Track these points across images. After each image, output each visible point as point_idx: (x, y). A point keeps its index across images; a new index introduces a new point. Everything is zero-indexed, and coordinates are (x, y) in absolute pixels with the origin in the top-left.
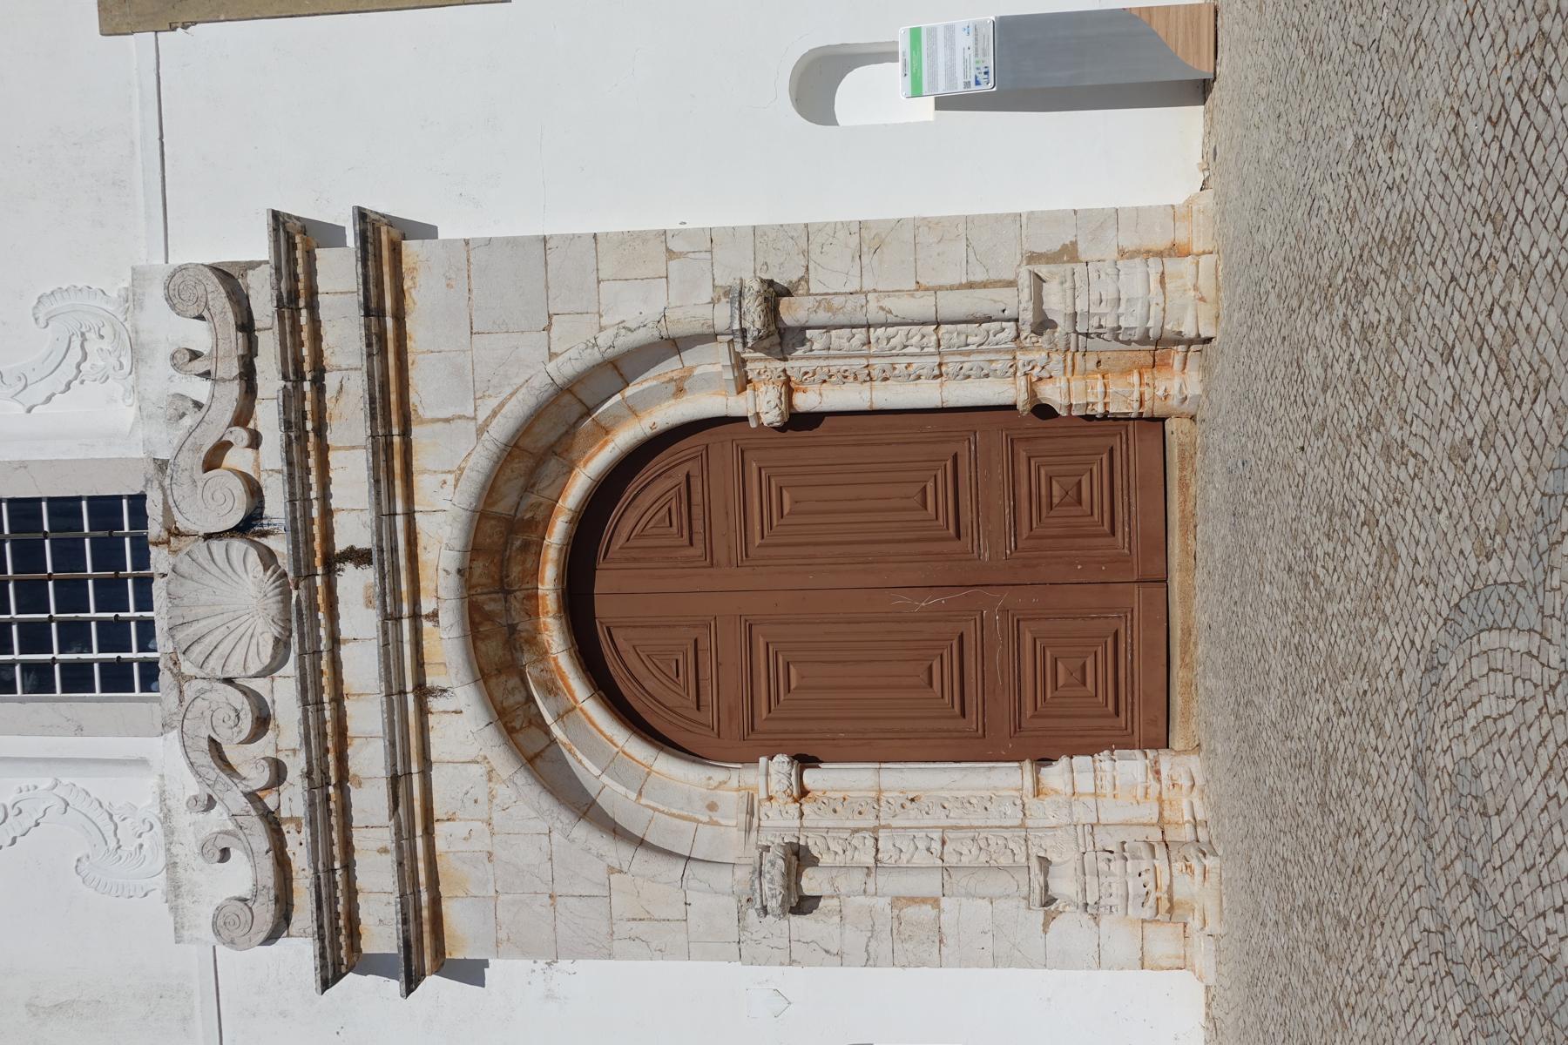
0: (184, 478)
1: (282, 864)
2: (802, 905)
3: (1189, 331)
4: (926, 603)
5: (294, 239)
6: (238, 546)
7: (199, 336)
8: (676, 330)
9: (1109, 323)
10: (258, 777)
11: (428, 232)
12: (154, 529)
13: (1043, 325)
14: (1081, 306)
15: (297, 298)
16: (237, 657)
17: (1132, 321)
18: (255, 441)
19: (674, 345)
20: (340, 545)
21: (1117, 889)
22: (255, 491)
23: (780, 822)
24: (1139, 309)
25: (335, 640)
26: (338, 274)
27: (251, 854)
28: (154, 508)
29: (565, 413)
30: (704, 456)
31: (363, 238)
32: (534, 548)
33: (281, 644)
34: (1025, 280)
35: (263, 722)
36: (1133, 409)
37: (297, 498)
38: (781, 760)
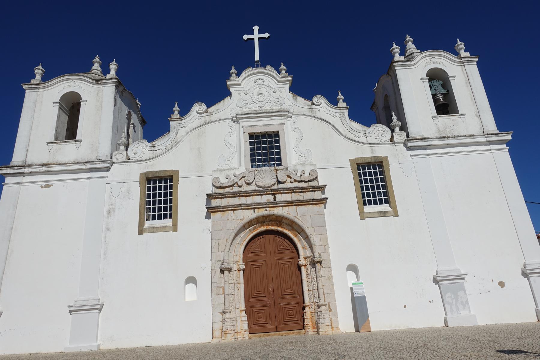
0: (285, 172)
1: (226, 187)
2: (222, 271)
3: (320, 330)
4: (271, 291)
5: (322, 188)
6: (276, 180)
7: (307, 174)
8: (313, 247)
9: (320, 317)
10: (240, 184)
11: (325, 208)
12: (277, 167)
13: (319, 306)
14: (323, 312)
17: (321, 321)
18: (292, 182)
19: (311, 247)
21: (228, 324)
22: (284, 183)
23: (235, 267)
24: (323, 322)
25: (261, 195)
26: (317, 195)
27: (228, 182)
28: (280, 167)
29: (293, 225)
31: (324, 199)
32: (277, 225)
33: (260, 187)
34: (326, 303)
36: (305, 323)
37: (284, 189)
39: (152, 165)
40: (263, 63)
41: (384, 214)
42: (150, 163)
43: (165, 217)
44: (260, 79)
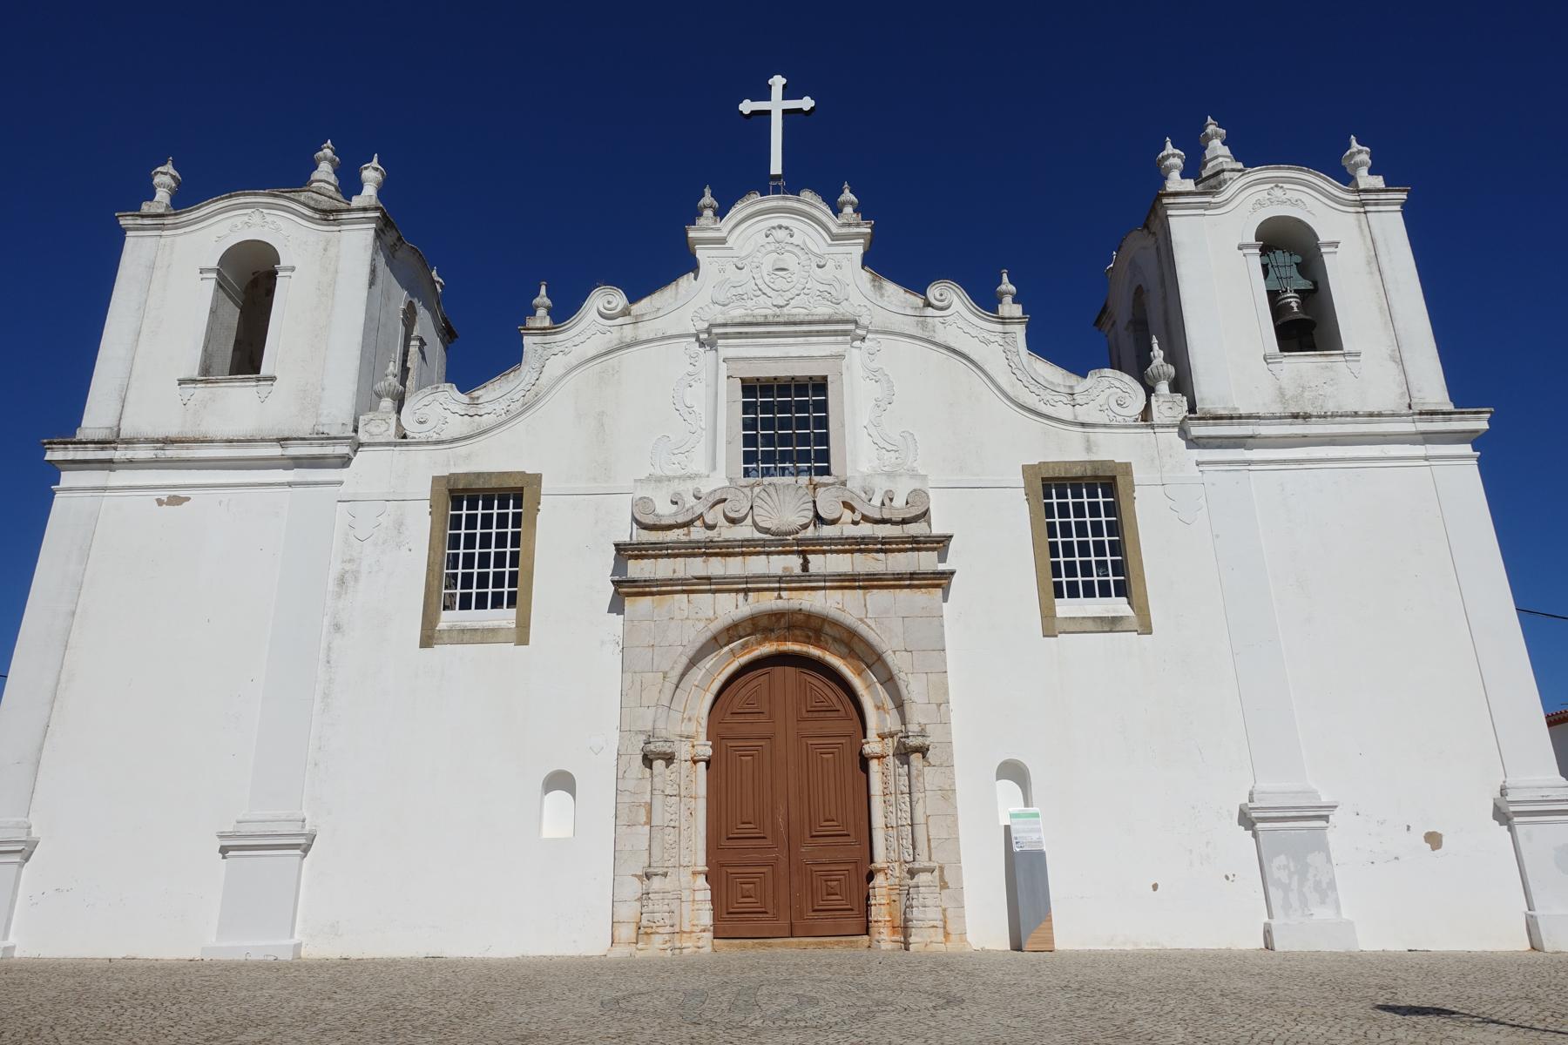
1: (669, 527)
2: (648, 761)
3: (912, 940)
5: (940, 544)
6: (811, 514)
7: (899, 502)
8: (907, 707)
9: (915, 903)
10: (709, 519)
11: (945, 599)
12: (817, 479)
13: (912, 873)
15: (917, 544)
16: (762, 512)
17: (916, 913)
18: (855, 523)
19: (900, 706)
20: (810, 557)
22: (834, 522)
23: (683, 751)
24: (921, 916)
25: (768, 554)
26: (926, 561)
27: (675, 514)
28: (825, 479)
30: (848, 718)
33: (767, 531)
34: (932, 864)
35: (733, 521)
36: (873, 918)
37: (831, 541)
38: (709, 752)
39: (468, 456)
41: (1111, 624)
42: (462, 449)
43: (497, 602)
44: (780, 227)
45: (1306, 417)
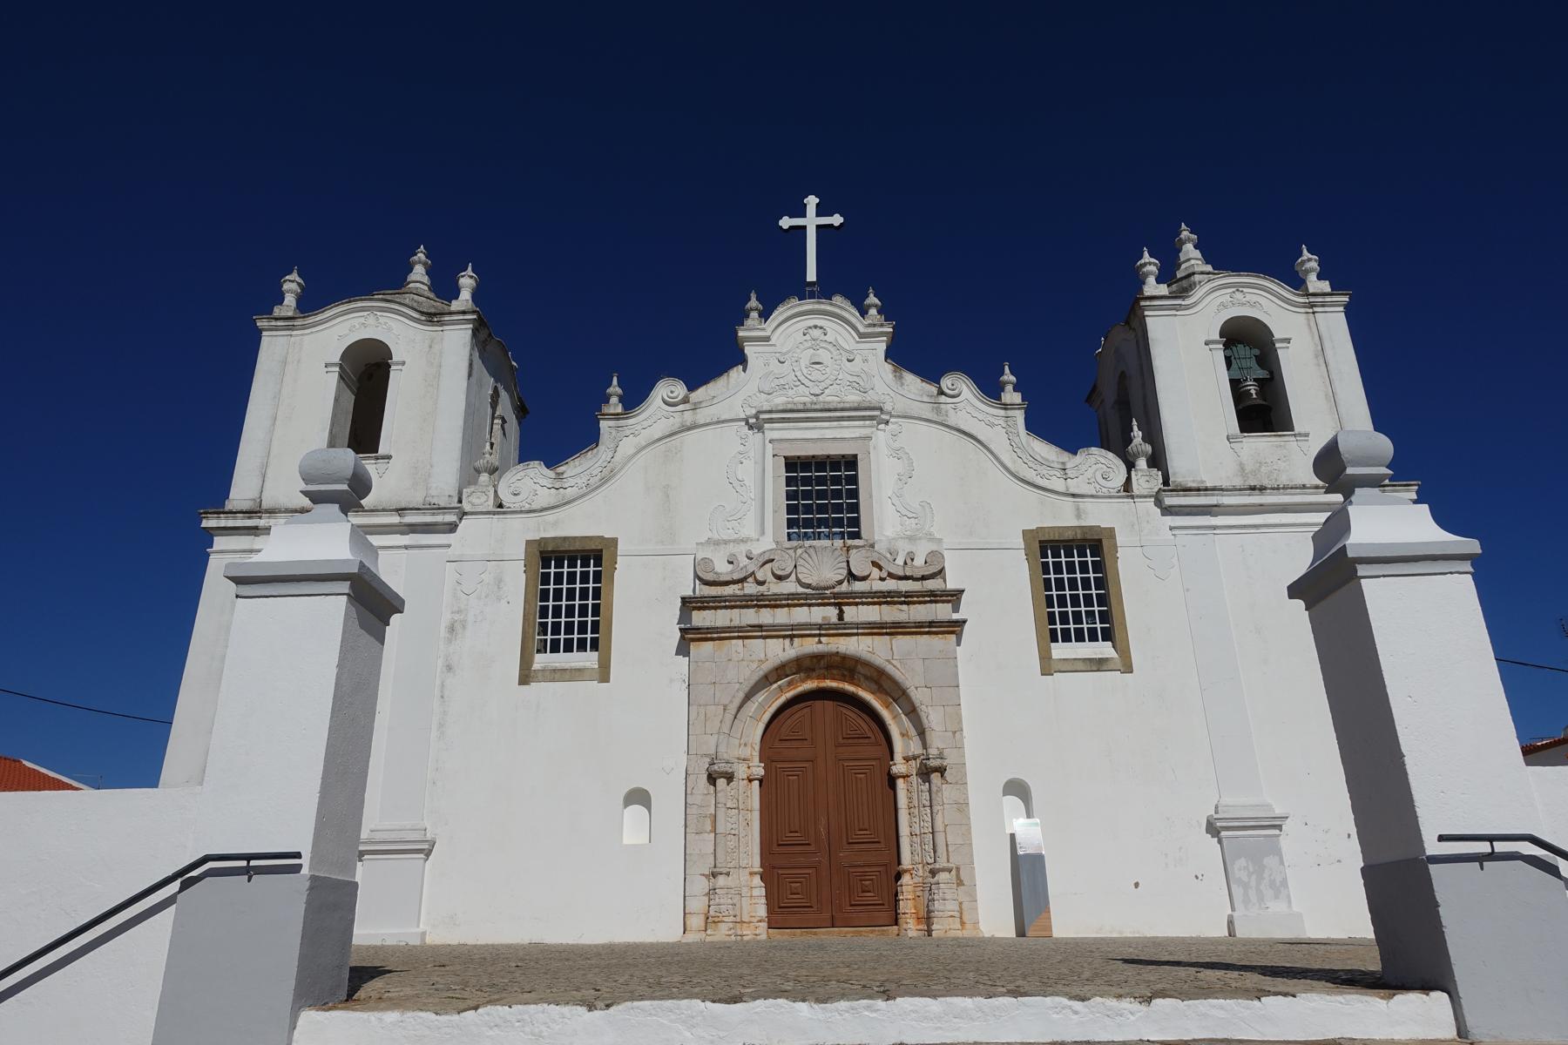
1: (727, 583)
2: (712, 779)
5: (954, 597)
7: (919, 561)
10: (760, 576)
11: (959, 644)
12: (850, 542)
13: (933, 873)
15: (934, 597)
18: (882, 579)
19: (922, 733)
22: (864, 579)
23: (741, 771)
25: (810, 605)
26: (942, 611)
27: (732, 572)
28: (856, 542)
30: (877, 744)
33: (808, 586)
35: (780, 578)
36: (901, 910)
37: (863, 594)
39: (555, 524)
40: (824, 290)
41: (1099, 664)
42: (550, 517)
45: (1262, 489)
